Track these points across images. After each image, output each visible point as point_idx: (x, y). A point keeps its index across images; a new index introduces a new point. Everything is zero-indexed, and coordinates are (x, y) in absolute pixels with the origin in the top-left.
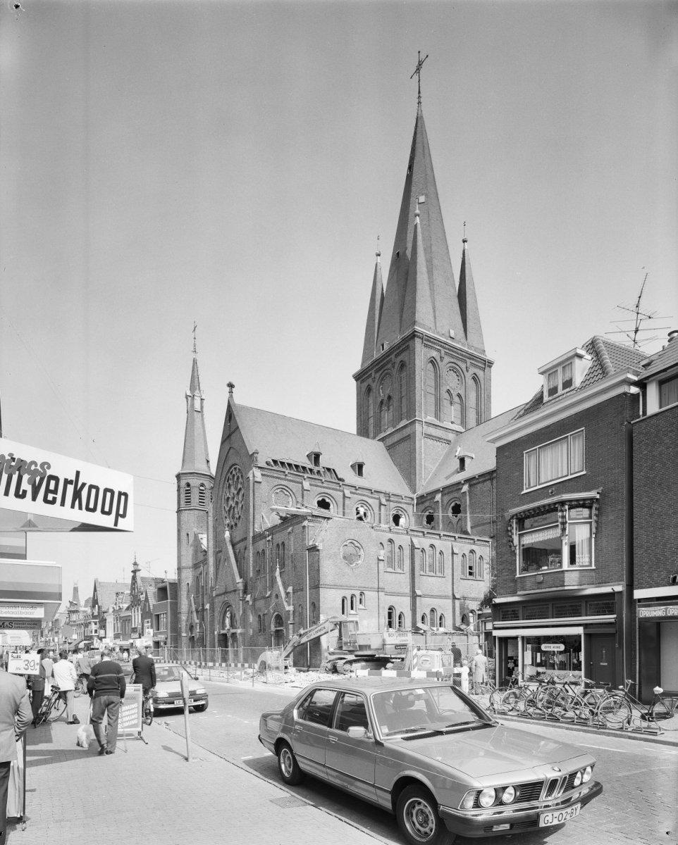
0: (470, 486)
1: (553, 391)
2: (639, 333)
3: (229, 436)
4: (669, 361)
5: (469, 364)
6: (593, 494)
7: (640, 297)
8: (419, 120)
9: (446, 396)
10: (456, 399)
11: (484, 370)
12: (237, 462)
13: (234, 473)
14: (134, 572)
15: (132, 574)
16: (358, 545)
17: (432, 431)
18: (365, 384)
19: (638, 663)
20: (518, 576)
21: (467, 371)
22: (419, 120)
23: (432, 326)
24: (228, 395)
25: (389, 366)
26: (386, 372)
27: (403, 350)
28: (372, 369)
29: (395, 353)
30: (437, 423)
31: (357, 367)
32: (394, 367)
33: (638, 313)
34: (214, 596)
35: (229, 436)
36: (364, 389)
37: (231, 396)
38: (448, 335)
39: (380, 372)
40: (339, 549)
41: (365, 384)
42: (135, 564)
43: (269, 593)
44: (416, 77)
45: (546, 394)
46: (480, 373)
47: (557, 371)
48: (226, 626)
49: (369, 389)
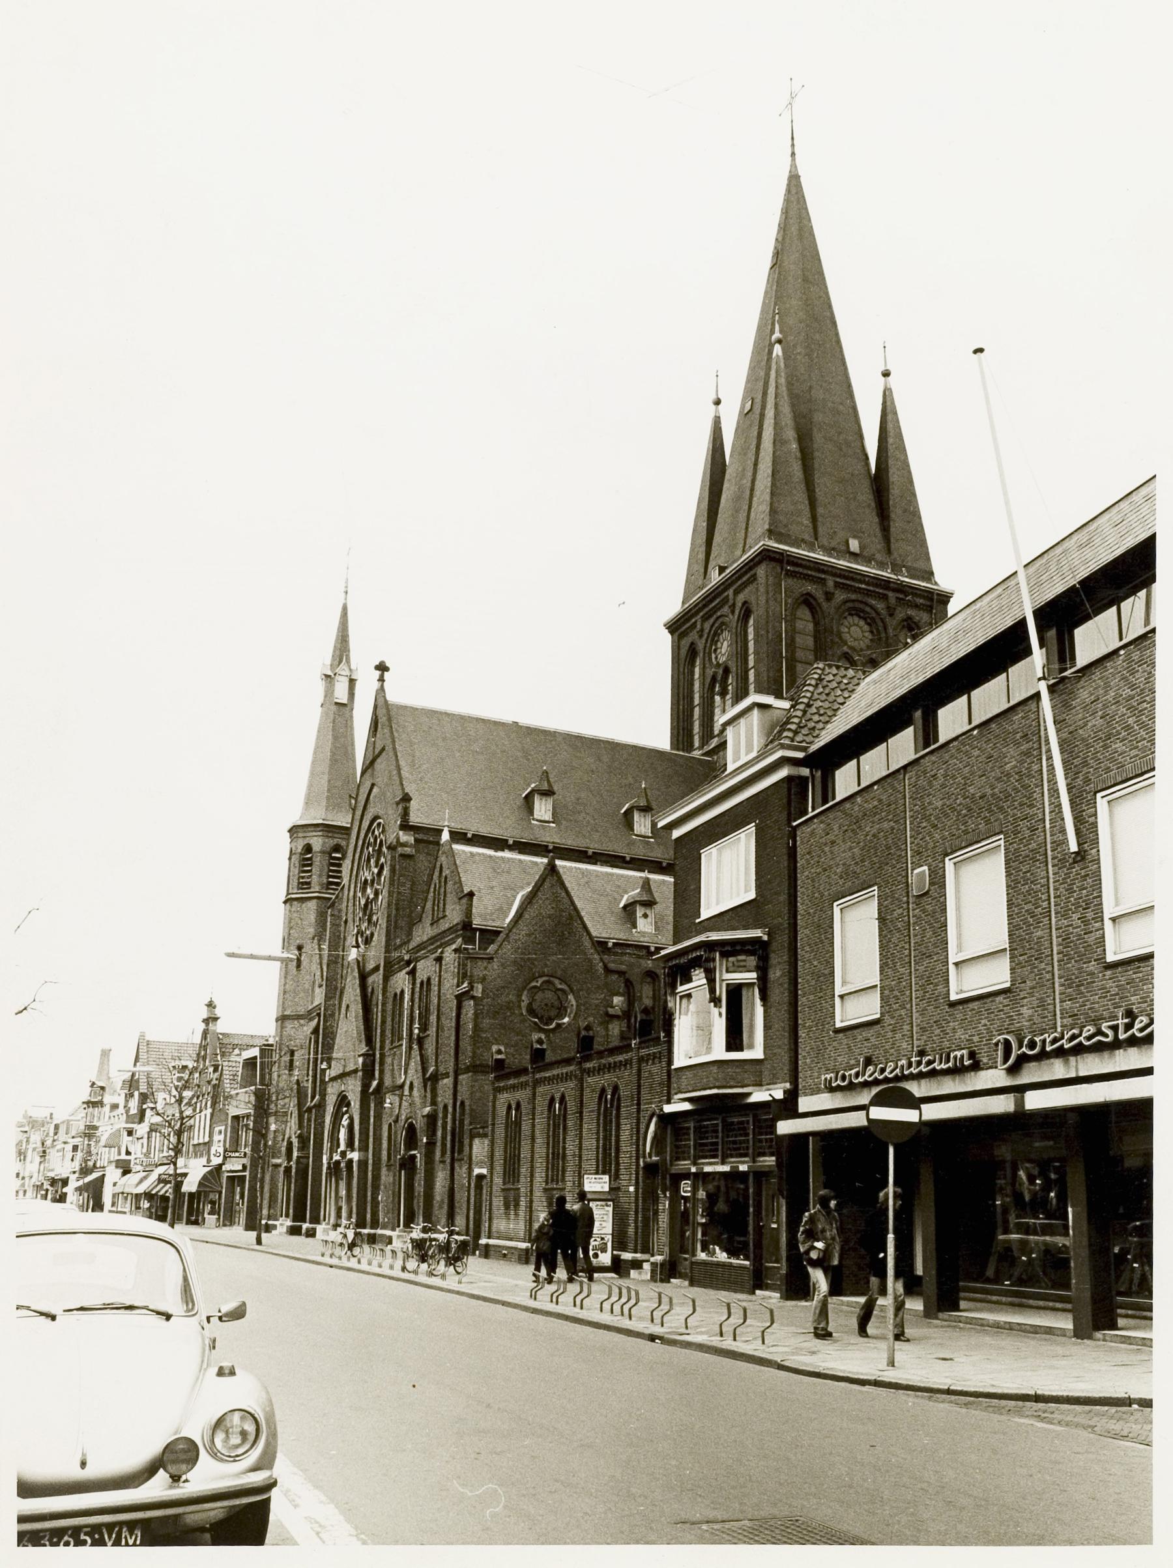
3: (372, 762)
5: (893, 601)
8: (345, 609)
12: (381, 813)
14: (206, 1021)
15: (203, 1026)
16: (563, 986)
18: (686, 643)
19: (370, 1174)
21: (891, 615)
22: (345, 609)
24: (377, 685)
26: (721, 620)
28: (697, 613)
29: (735, 587)
31: (674, 607)
32: (733, 612)
35: (372, 762)
36: (684, 652)
37: (382, 688)
39: (712, 620)
40: (519, 996)
41: (686, 643)
42: (211, 1005)
48: (338, 1146)
49: (693, 652)
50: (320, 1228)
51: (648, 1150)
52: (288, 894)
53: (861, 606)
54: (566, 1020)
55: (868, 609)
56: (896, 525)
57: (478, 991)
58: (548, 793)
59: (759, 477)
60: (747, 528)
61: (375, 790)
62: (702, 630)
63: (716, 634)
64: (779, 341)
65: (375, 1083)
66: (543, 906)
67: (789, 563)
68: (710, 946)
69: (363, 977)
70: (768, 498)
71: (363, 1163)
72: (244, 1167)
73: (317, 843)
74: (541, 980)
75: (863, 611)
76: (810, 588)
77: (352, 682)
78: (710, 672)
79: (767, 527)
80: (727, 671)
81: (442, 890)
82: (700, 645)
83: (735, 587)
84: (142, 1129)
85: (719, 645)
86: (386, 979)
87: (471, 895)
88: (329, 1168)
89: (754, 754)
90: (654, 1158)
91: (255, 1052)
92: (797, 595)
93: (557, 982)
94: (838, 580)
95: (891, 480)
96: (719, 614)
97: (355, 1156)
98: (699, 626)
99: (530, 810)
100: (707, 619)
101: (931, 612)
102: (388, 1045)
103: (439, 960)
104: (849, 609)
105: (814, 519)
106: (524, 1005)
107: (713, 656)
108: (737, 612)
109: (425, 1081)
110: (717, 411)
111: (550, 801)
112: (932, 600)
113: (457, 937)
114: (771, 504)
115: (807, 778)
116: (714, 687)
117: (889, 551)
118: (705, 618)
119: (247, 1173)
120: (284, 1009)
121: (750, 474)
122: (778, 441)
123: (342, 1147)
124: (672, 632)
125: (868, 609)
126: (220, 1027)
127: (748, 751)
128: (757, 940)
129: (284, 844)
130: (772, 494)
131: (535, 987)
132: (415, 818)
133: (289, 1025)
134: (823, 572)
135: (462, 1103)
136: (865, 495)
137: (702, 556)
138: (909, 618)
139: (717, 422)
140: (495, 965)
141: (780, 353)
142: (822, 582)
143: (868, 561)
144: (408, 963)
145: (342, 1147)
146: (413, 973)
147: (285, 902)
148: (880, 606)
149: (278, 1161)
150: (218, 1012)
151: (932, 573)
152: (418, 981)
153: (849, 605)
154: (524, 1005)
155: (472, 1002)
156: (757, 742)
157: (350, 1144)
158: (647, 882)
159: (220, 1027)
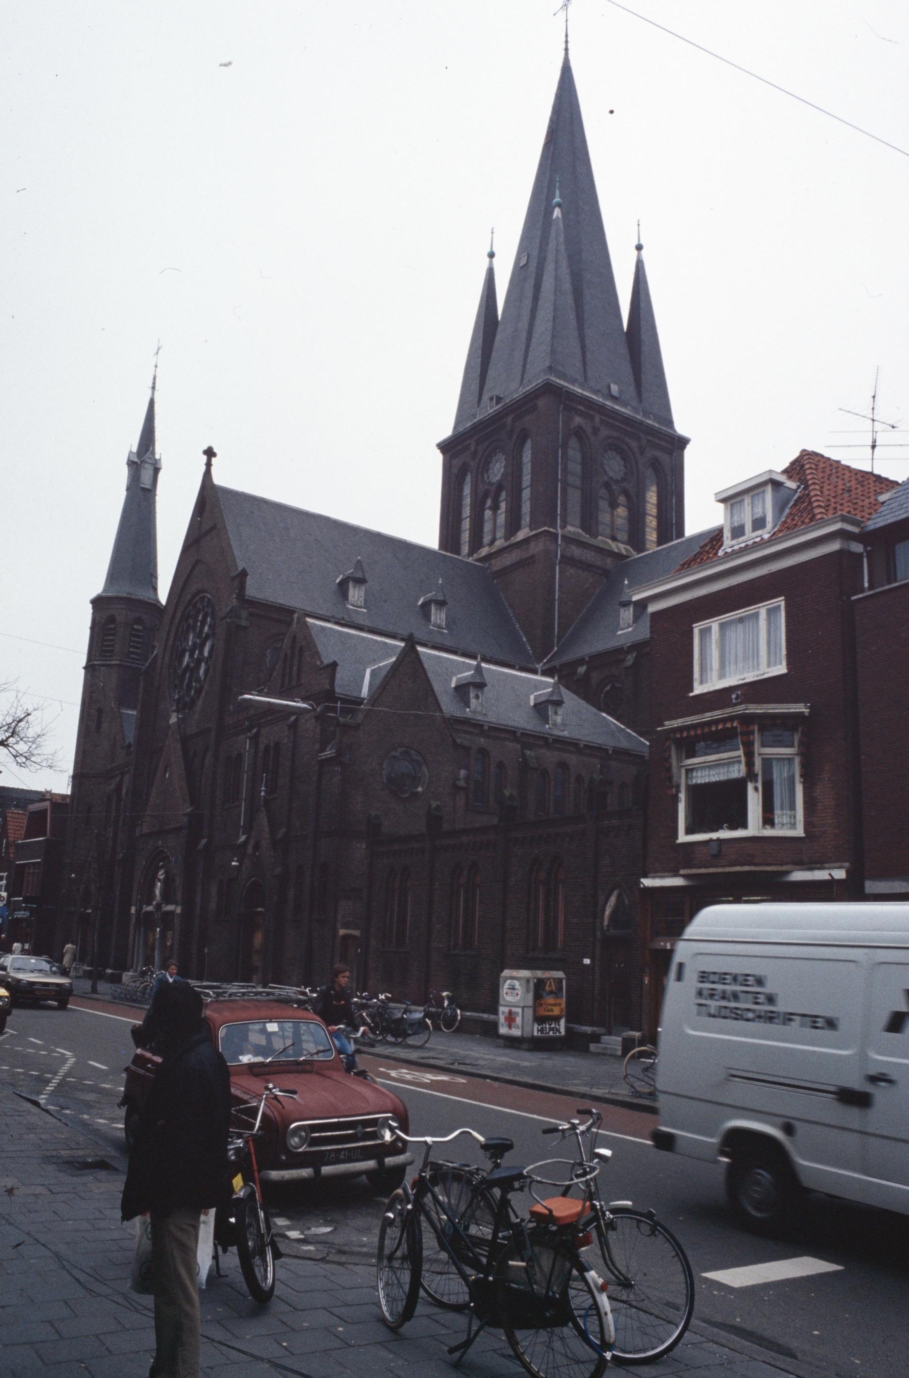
1: (738, 532)
2: (876, 449)
4: (900, 512)
6: (801, 708)
7: (874, 397)
9: (603, 492)
10: (622, 499)
11: (671, 453)
13: (199, 606)
16: (419, 758)
17: (577, 552)
20: (683, 838)
21: (642, 453)
23: (580, 378)
30: (586, 537)
31: (446, 430)
33: (873, 420)
34: (137, 835)
36: (455, 471)
38: (605, 391)
41: (457, 463)
43: (243, 838)
44: (562, 15)
45: (727, 534)
46: (664, 458)
47: (743, 500)
49: (464, 470)
50: (127, 976)
55: (625, 447)
58: (360, 581)
59: (538, 321)
68: (747, 720)
70: (549, 338)
74: (400, 750)
77: (157, 470)
81: (296, 661)
87: (334, 665)
88: (138, 918)
94: (603, 418)
95: (643, 337)
98: (473, 448)
105: (584, 364)
107: (486, 476)
110: (491, 263)
115: (861, 555)
117: (640, 400)
121: (526, 319)
122: (557, 291)
130: (553, 336)
131: (394, 757)
136: (623, 350)
138: (656, 459)
141: (560, 216)
142: (592, 418)
143: (625, 405)
144: (250, 729)
146: (255, 739)
148: (634, 444)
152: (262, 747)
157: (167, 897)
158: (478, 669)
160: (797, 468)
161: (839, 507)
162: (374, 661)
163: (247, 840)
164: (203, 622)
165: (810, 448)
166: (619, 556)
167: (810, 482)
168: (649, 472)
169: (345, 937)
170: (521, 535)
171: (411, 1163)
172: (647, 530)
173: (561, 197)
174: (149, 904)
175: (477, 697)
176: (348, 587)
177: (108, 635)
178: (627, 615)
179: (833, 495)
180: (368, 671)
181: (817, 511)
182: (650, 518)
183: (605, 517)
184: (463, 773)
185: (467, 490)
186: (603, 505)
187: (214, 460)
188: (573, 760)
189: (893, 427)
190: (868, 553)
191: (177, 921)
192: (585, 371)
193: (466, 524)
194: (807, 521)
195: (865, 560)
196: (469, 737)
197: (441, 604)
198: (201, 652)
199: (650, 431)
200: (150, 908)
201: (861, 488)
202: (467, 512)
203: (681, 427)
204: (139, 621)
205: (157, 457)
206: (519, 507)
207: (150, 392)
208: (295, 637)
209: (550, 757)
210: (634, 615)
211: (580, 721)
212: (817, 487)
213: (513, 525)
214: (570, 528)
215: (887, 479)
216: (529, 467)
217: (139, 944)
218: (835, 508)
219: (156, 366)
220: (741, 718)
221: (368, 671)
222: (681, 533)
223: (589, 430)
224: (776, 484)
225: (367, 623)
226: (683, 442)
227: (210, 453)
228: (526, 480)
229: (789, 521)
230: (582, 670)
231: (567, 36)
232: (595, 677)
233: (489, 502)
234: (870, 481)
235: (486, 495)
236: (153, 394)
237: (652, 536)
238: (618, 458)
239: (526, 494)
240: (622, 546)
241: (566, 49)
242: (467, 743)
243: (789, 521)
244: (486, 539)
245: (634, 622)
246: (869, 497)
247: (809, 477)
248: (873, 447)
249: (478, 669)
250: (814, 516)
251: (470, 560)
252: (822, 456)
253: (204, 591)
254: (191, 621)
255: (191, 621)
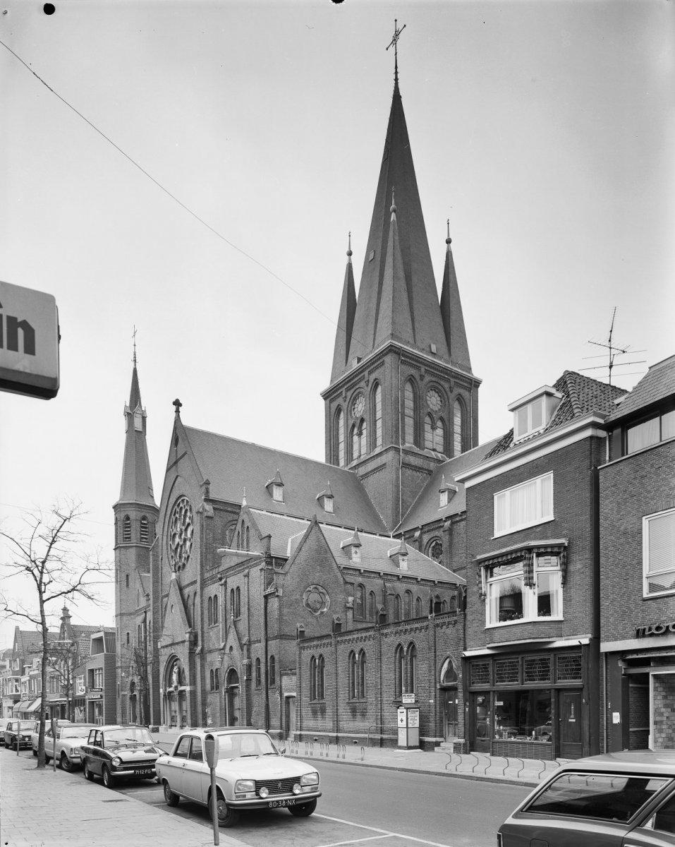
0: (453, 523)
3: (176, 463)
5: (452, 383)
7: (611, 331)
9: (427, 419)
10: (439, 424)
15: (61, 622)
16: (324, 591)
21: (451, 391)
23: (412, 341)
24: (174, 415)
25: (363, 384)
27: (377, 368)
30: (416, 450)
31: (326, 384)
32: (367, 385)
33: (610, 348)
35: (176, 463)
36: (333, 410)
40: (301, 596)
41: (334, 405)
44: (392, 49)
46: (465, 394)
51: (442, 678)
52: (116, 545)
53: (437, 385)
54: (325, 610)
55: (440, 387)
56: (454, 338)
57: (280, 593)
58: (280, 485)
60: (375, 334)
61: (179, 479)
62: (346, 397)
63: (355, 399)
64: (394, 211)
65: (199, 648)
66: (312, 542)
67: (403, 355)
69: (181, 589)
71: (193, 693)
72: (101, 697)
73: (133, 514)
75: (438, 388)
76: (413, 371)
77: (144, 418)
78: (351, 422)
79: (390, 332)
80: (362, 420)
82: (344, 406)
83: (369, 370)
84: (25, 679)
85: (356, 406)
86: (202, 589)
87: (269, 537)
88: (165, 695)
89: (541, 429)
90: (445, 683)
91: (102, 634)
92: (406, 375)
93: (320, 588)
94: (427, 368)
96: (357, 387)
97: (188, 688)
99: (271, 495)
100: (350, 389)
101: (470, 391)
102: (206, 625)
103: (247, 576)
104: (432, 386)
106: (304, 601)
107: (353, 413)
108: (370, 386)
109: (242, 646)
110: (350, 259)
111: (281, 488)
112: (471, 384)
113: (262, 561)
114: (393, 318)
116: (353, 431)
118: (348, 390)
119: (104, 700)
120: (121, 610)
123: (175, 684)
124: (325, 399)
125: (440, 387)
126: (73, 621)
127: (536, 424)
128: (559, 546)
129: (111, 516)
132: (212, 496)
133: (125, 618)
134: (420, 363)
135: (272, 657)
137: (344, 352)
139: (350, 267)
140: (288, 577)
141: (395, 219)
143: (441, 358)
144: (221, 579)
145: (175, 684)
147: (115, 549)
148: (446, 386)
149: (126, 693)
150: (70, 613)
151: (471, 369)
153: (431, 384)
154: (304, 601)
155: (276, 599)
156: (545, 421)
157: (180, 682)
159: (73, 621)
160: (561, 384)
161: (590, 408)
162: (293, 534)
163: (225, 646)
164: (185, 516)
165: (571, 370)
166: (439, 461)
167: (571, 392)
168: (456, 405)
169: (288, 698)
170: (378, 450)
171: (319, 795)
172: (455, 443)
173: (396, 204)
174: (170, 686)
175: (356, 553)
176: (272, 489)
177: (126, 527)
178: (444, 498)
179: (586, 400)
180: (290, 540)
181: (575, 411)
182: (457, 435)
183: (428, 435)
184: (351, 599)
185: (342, 422)
186: (427, 427)
187: (181, 409)
188: (414, 588)
189: (624, 352)
190: (609, 436)
191: (188, 695)
192: (414, 336)
193: (342, 446)
194: (569, 418)
195: (607, 442)
196: (352, 577)
197: (331, 497)
198: (186, 535)
199: (457, 376)
200: (171, 689)
201: (603, 396)
202: (342, 438)
203: (476, 373)
204: (144, 518)
205: (143, 409)
206: (375, 432)
207: (133, 363)
208: (243, 521)
209: (401, 587)
210: (448, 498)
211: (416, 564)
212: (576, 395)
213: (373, 444)
214: (407, 445)
215: (619, 389)
216: (381, 405)
217: (500, 660)
218: (587, 409)
219: (135, 345)
220: (520, 553)
221: (290, 540)
222: (476, 444)
223: (418, 378)
224: (549, 394)
225: (286, 511)
226: (477, 383)
227: (177, 404)
228: (379, 414)
229: (557, 420)
230: (417, 534)
231: (396, 67)
232: (426, 538)
233: (356, 431)
234: (609, 390)
235: (354, 426)
236: (135, 365)
237: (457, 446)
238: (436, 395)
239: (379, 424)
240: (439, 455)
241: (396, 79)
242: (352, 581)
243: (557, 420)
244: (355, 455)
245: (449, 502)
246: (609, 401)
247: (570, 389)
248: (611, 367)
249: (356, 536)
250: (574, 415)
251: (346, 469)
252: (578, 374)
253: (185, 496)
254: (177, 516)
255: (177, 516)
